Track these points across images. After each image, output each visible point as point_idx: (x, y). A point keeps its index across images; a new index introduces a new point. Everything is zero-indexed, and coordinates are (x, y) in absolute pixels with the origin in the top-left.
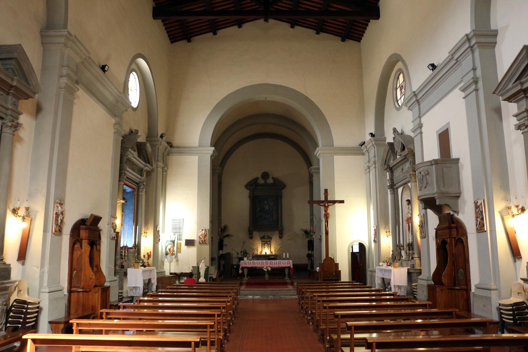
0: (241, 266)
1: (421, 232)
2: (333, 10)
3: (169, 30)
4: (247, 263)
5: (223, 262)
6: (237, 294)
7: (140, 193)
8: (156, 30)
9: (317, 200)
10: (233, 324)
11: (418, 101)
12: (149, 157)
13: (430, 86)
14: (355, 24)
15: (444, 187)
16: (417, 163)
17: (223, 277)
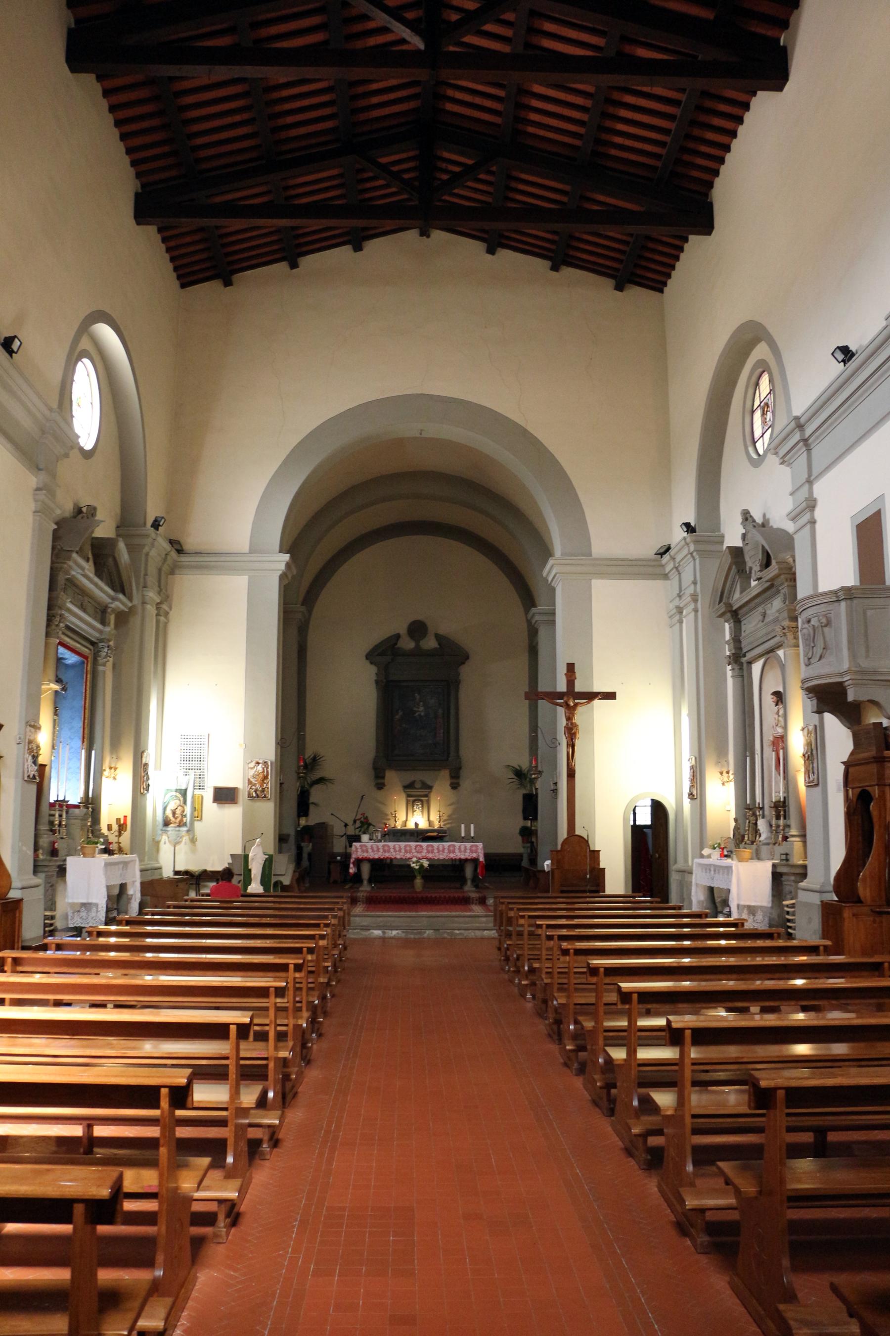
0: (354, 856)
1: (807, 772)
2: (596, 208)
3: (177, 253)
4: (368, 848)
5: (308, 847)
6: (343, 923)
7: (101, 668)
8: (143, 252)
9: (548, 690)
10: (333, 996)
11: (805, 441)
12: (124, 577)
13: (836, 404)
14: (651, 245)
15: (867, 657)
16: (800, 595)
17: (307, 885)
